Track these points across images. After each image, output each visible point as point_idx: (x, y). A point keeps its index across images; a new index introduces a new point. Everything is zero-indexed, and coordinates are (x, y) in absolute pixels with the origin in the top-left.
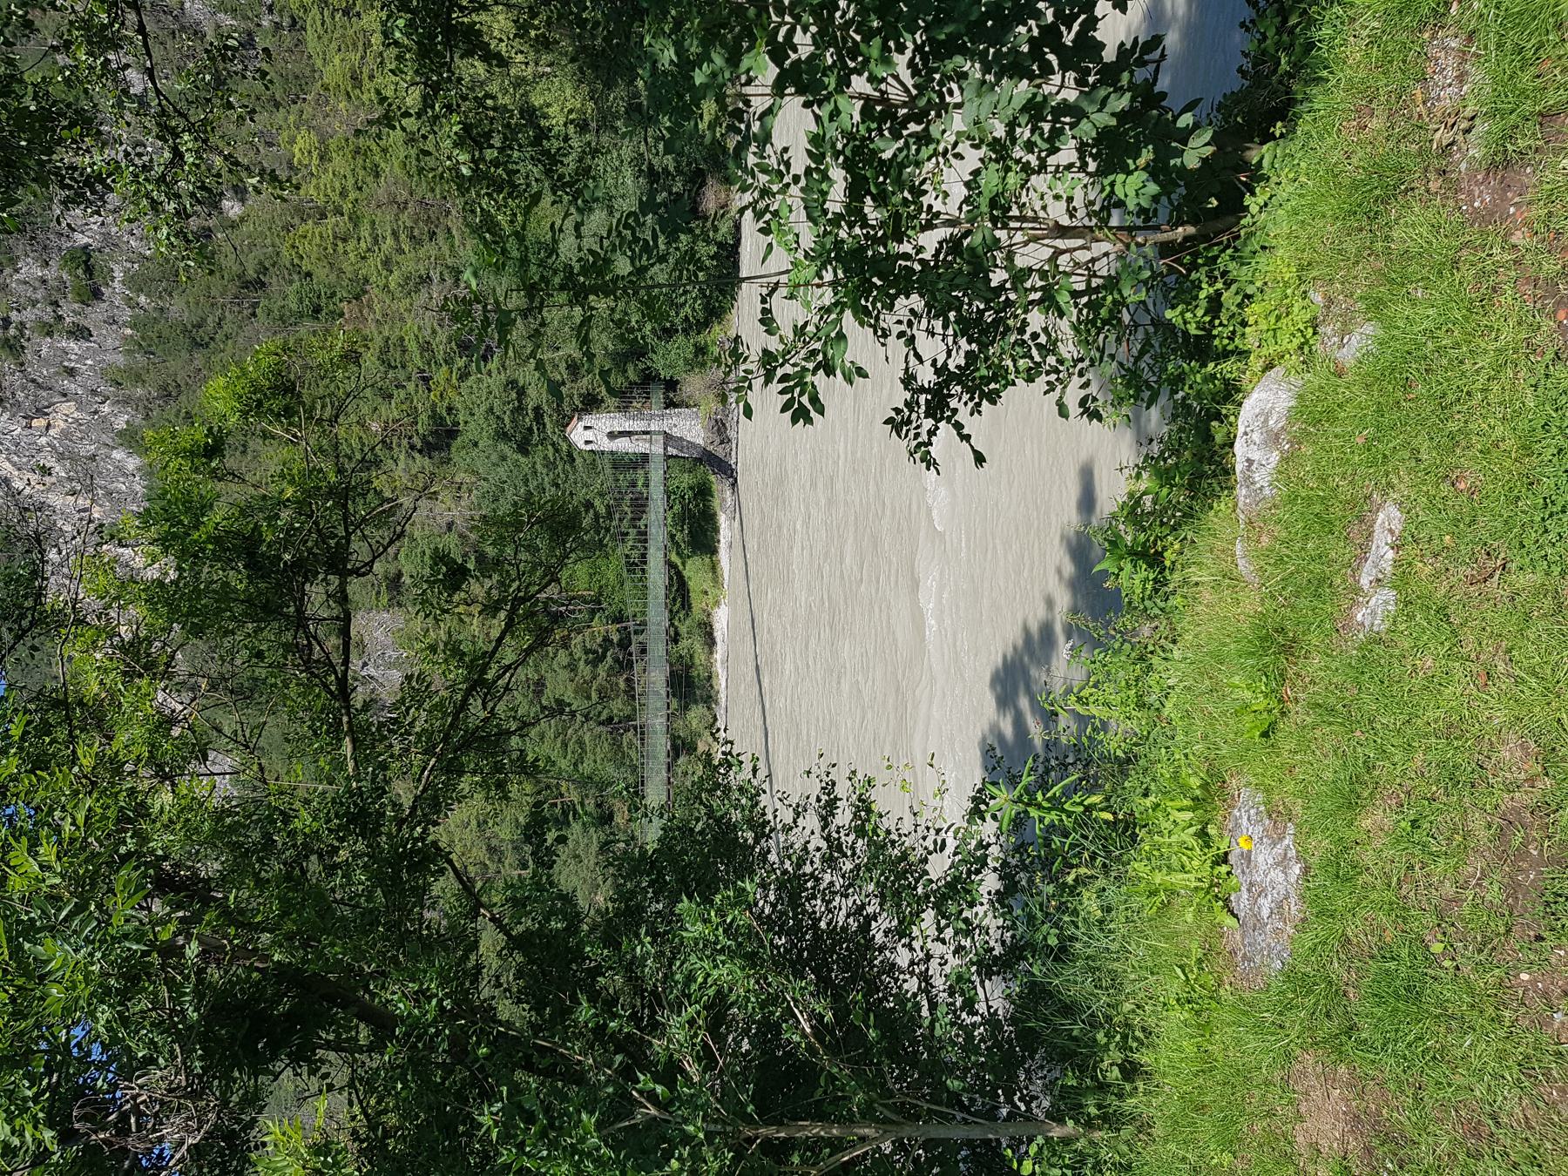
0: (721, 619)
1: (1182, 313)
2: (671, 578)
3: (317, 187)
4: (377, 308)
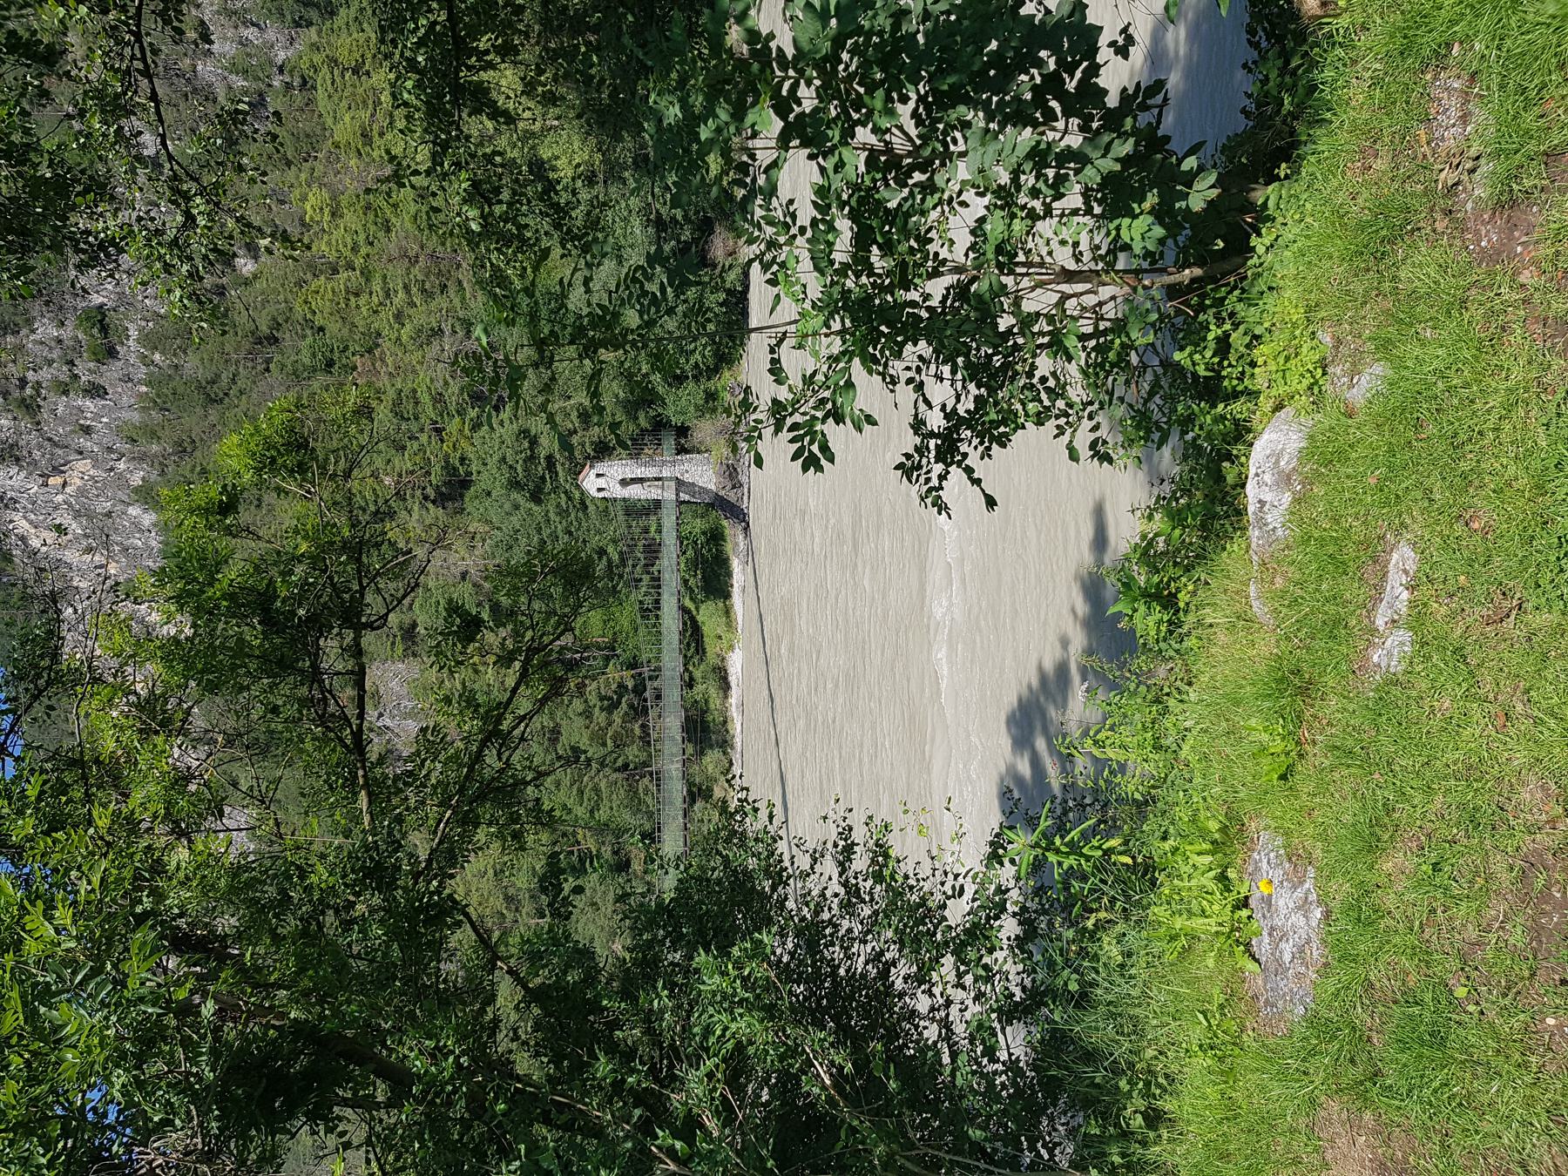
0: (736, 664)
1: (1191, 355)
2: (685, 624)
3: (329, 243)
4: (389, 361)
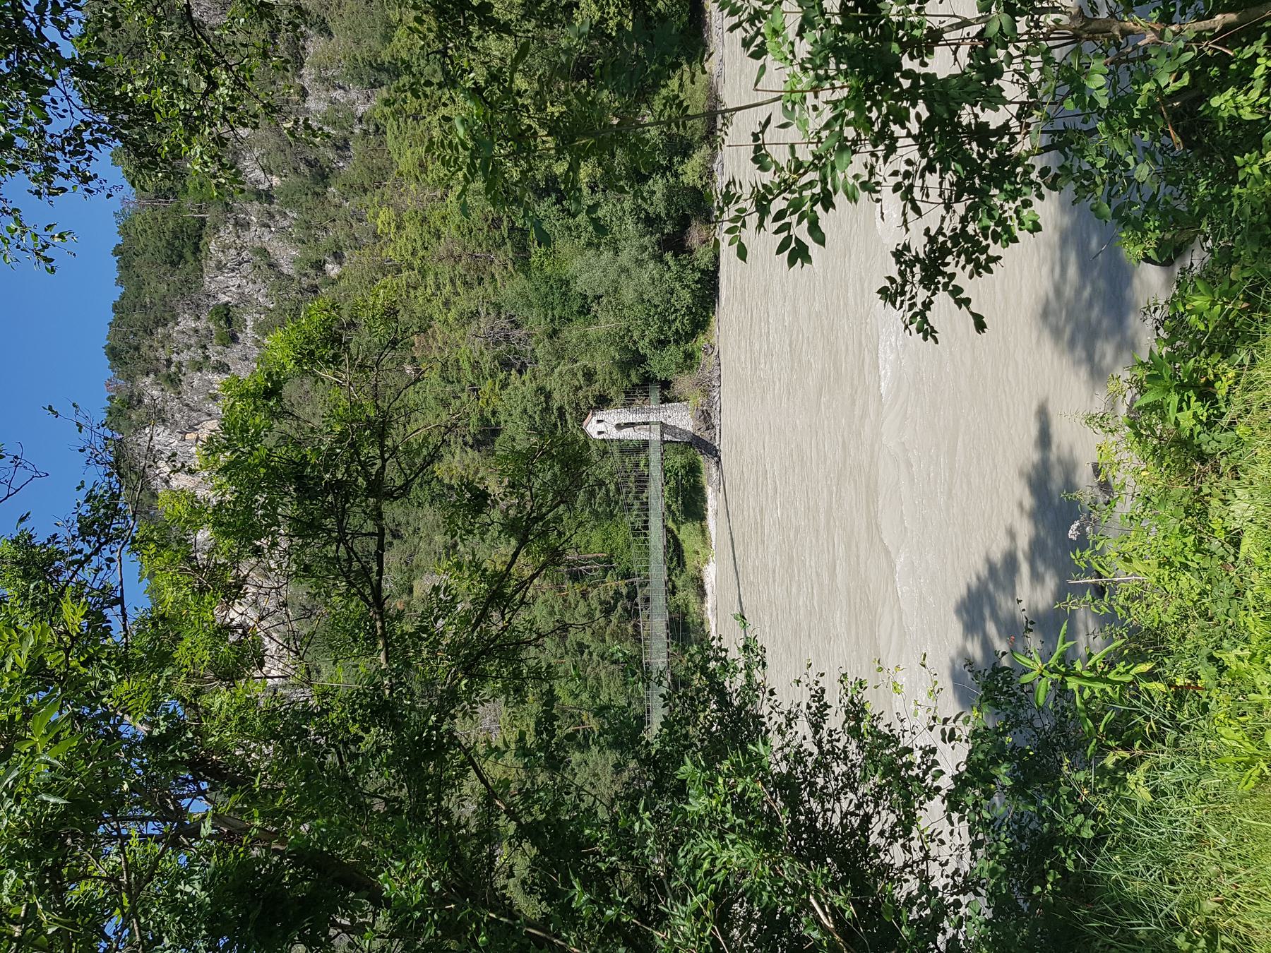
0: (711, 575)
1: (1233, 97)
2: (668, 541)
3: (394, 249)
4: (439, 338)
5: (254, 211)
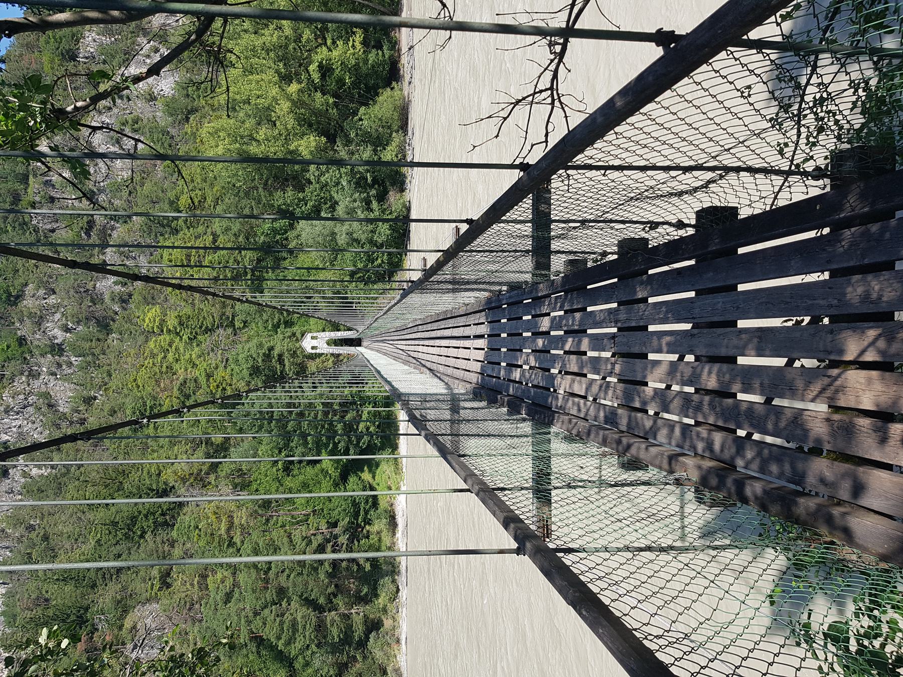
5: (46, 363)
